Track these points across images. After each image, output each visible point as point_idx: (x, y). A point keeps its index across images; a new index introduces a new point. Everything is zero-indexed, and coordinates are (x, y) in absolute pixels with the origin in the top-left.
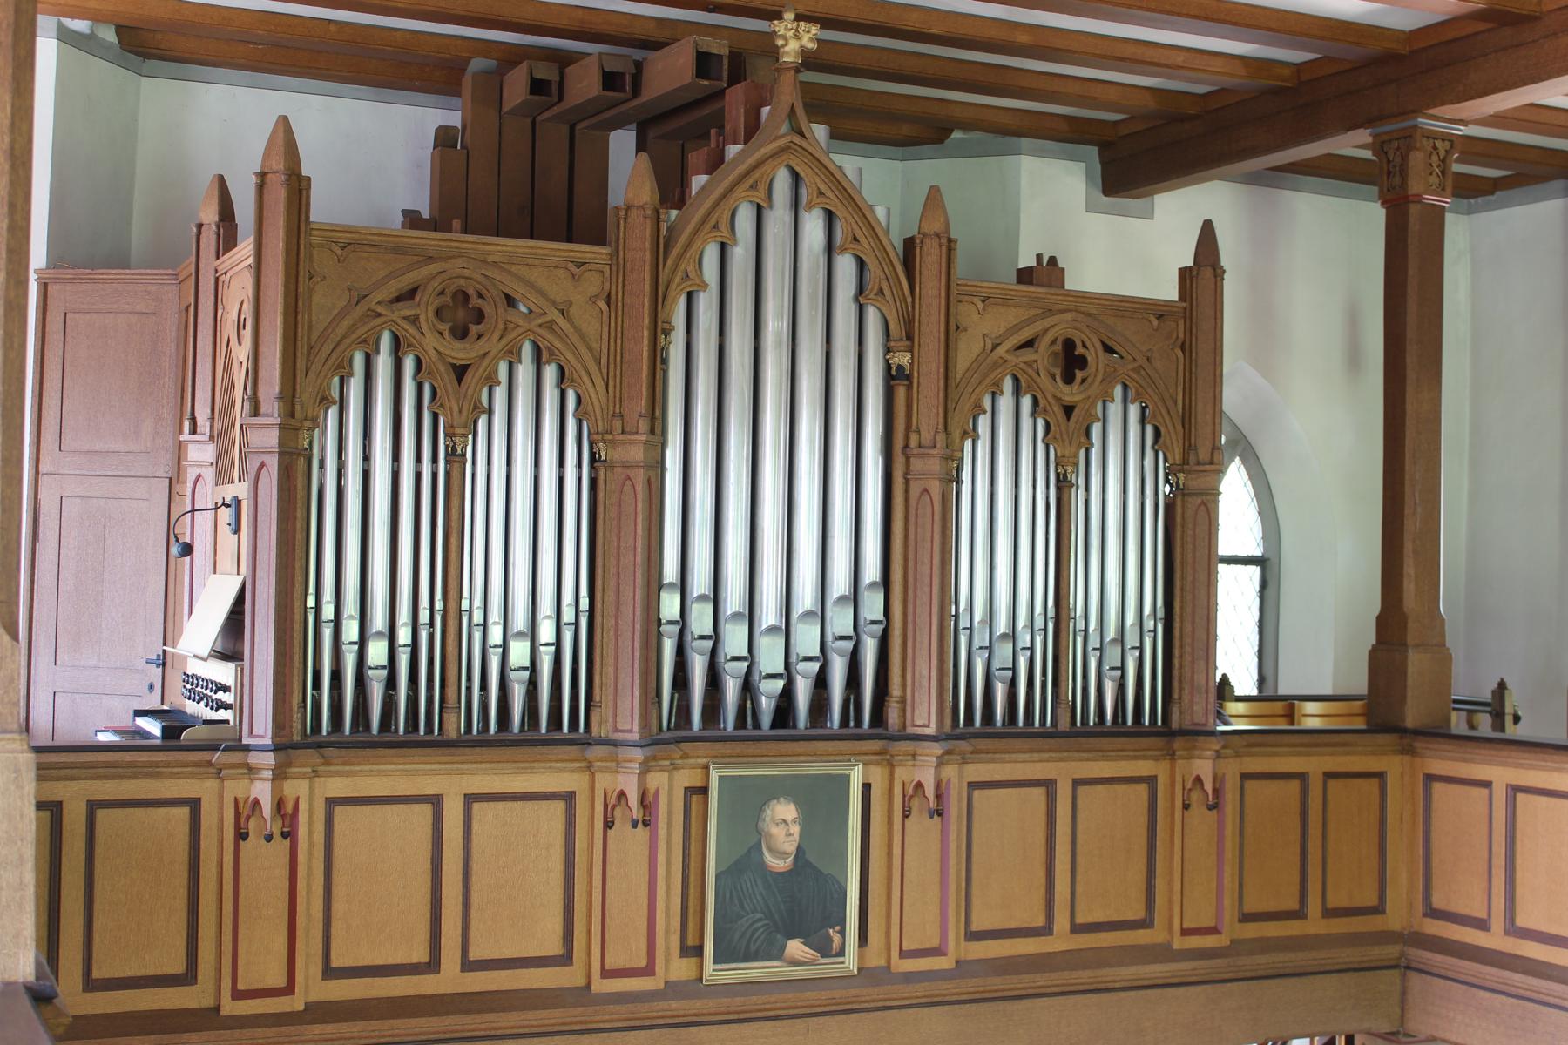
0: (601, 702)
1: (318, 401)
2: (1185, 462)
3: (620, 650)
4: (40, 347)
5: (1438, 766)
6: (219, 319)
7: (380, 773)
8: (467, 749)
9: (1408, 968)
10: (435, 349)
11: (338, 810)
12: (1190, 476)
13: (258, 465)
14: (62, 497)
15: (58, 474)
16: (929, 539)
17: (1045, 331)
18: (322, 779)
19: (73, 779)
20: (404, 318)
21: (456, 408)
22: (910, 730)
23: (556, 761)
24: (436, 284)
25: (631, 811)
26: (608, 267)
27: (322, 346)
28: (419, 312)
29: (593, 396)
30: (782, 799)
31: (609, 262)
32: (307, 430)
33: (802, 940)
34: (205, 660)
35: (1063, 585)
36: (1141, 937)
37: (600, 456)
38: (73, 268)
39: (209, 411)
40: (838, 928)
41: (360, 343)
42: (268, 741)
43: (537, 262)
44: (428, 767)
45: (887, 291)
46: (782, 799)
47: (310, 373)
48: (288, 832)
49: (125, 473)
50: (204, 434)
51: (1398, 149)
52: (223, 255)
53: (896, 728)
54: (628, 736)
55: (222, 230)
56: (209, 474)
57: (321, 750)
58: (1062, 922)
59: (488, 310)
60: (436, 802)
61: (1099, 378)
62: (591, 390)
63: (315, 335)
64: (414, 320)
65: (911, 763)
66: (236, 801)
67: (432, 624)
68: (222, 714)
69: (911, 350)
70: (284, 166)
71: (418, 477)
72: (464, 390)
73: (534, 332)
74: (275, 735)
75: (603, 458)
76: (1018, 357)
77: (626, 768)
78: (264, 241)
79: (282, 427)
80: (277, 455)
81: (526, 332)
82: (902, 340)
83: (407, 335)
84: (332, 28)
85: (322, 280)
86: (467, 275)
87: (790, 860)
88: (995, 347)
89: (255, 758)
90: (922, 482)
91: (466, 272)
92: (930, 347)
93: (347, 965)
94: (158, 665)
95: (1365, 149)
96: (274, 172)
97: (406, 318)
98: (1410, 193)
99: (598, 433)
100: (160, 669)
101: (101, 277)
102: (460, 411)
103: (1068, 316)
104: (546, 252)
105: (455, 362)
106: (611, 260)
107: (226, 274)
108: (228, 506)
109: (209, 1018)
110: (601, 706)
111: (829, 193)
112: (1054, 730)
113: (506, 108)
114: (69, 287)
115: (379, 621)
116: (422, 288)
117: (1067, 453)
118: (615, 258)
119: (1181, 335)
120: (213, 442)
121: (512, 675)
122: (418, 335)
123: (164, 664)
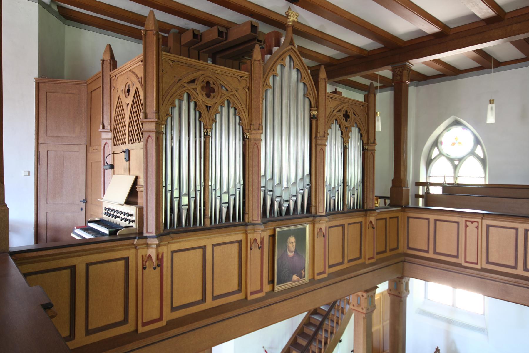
0: (248, 212)
1: (166, 115)
2: (368, 143)
3: (254, 196)
4: (37, 103)
5: (411, 215)
6: (112, 91)
7: (188, 241)
8: (213, 230)
9: (405, 261)
10: (202, 100)
11: (174, 254)
12: (369, 146)
13: (147, 136)
14: (47, 151)
15: (46, 144)
16: (323, 162)
17: (343, 108)
18: (170, 245)
19: (80, 256)
20: (192, 89)
21: (208, 120)
22: (318, 214)
23: (237, 231)
24: (201, 79)
25: (258, 244)
26: (248, 79)
27: (167, 96)
28: (197, 87)
29: (245, 118)
30: (292, 236)
31: (248, 77)
32: (163, 125)
33: (296, 275)
34: (123, 205)
35: (345, 174)
36: (360, 261)
37: (247, 137)
38: (48, 78)
39: (109, 122)
40: (304, 270)
41: (178, 96)
42: (155, 235)
43: (229, 75)
44: (202, 237)
45: (311, 94)
46: (292, 236)
47: (163, 105)
48: (160, 265)
49: (70, 143)
50: (108, 129)
51: (399, 70)
52: (113, 70)
53: (314, 213)
54: (257, 222)
55: (112, 62)
56: (110, 143)
57: (170, 235)
58: (346, 261)
59: (216, 89)
60: (204, 248)
61: (353, 121)
62: (244, 116)
63: (164, 92)
64: (195, 89)
65: (319, 223)
66: (142, 256)
67: (200, 190)
68: (131, 224)
69: (317, 110)
70: (154, 28)
71: (196, 142)
72: (210, 114)
73: (229, 97)
74: (156, 232)
75: (248, 138)
76: (338, 114)
77: (257, 232)
78: (147, 55)
79: (157, 123)
80: (155, 133)
81: (226, 97)
82: (314, 107)
83: (193, 95)
84: (131, 14)
85: (166, 73)
86: (211, 76)
87: (293, 253)
88: (333, 111)
89: (149, 241)
90: (321, 147)
91: (211, 76)
92: (323, 110)
93: (178, 305)
94: (84, 202)
95: (362, 77)
96: (151, 30)
97: (193, 89)
98: (403, 80)
99: (246, 130)
100: (85, 204)
101: (59, 81)
102: (209, 121)
103: (347, 104)
104: (232, 72)
105: (207, 105)
106: (249, 76)
107: (115, 76)
108: (124, 152)
109: (134, 335)
110: (248, 213)
111: (299, 64)
112: (343, 211)
113: (181, 45)
114: (47, 84)
115: (185, 191)
116: (197, 79)
117: (346, 140)
118: (250, 76)
119: (366, 111)
120: (111, 132)
121: (224, 205)
122: (197, 95)
123: (86, 202)
